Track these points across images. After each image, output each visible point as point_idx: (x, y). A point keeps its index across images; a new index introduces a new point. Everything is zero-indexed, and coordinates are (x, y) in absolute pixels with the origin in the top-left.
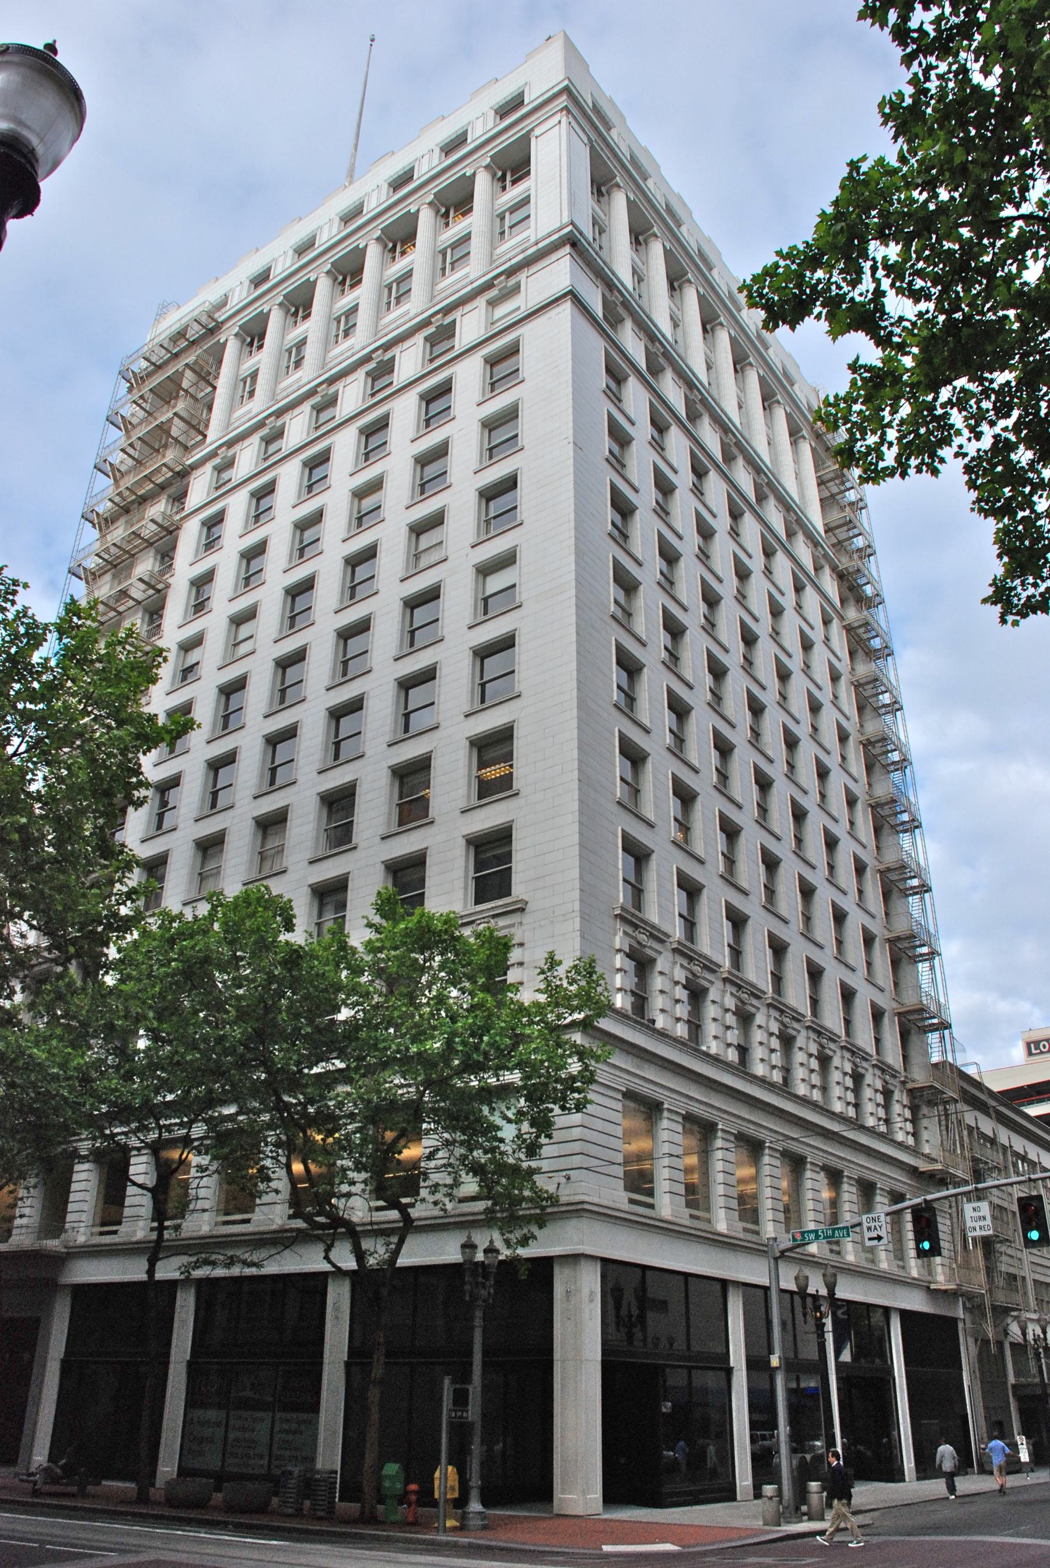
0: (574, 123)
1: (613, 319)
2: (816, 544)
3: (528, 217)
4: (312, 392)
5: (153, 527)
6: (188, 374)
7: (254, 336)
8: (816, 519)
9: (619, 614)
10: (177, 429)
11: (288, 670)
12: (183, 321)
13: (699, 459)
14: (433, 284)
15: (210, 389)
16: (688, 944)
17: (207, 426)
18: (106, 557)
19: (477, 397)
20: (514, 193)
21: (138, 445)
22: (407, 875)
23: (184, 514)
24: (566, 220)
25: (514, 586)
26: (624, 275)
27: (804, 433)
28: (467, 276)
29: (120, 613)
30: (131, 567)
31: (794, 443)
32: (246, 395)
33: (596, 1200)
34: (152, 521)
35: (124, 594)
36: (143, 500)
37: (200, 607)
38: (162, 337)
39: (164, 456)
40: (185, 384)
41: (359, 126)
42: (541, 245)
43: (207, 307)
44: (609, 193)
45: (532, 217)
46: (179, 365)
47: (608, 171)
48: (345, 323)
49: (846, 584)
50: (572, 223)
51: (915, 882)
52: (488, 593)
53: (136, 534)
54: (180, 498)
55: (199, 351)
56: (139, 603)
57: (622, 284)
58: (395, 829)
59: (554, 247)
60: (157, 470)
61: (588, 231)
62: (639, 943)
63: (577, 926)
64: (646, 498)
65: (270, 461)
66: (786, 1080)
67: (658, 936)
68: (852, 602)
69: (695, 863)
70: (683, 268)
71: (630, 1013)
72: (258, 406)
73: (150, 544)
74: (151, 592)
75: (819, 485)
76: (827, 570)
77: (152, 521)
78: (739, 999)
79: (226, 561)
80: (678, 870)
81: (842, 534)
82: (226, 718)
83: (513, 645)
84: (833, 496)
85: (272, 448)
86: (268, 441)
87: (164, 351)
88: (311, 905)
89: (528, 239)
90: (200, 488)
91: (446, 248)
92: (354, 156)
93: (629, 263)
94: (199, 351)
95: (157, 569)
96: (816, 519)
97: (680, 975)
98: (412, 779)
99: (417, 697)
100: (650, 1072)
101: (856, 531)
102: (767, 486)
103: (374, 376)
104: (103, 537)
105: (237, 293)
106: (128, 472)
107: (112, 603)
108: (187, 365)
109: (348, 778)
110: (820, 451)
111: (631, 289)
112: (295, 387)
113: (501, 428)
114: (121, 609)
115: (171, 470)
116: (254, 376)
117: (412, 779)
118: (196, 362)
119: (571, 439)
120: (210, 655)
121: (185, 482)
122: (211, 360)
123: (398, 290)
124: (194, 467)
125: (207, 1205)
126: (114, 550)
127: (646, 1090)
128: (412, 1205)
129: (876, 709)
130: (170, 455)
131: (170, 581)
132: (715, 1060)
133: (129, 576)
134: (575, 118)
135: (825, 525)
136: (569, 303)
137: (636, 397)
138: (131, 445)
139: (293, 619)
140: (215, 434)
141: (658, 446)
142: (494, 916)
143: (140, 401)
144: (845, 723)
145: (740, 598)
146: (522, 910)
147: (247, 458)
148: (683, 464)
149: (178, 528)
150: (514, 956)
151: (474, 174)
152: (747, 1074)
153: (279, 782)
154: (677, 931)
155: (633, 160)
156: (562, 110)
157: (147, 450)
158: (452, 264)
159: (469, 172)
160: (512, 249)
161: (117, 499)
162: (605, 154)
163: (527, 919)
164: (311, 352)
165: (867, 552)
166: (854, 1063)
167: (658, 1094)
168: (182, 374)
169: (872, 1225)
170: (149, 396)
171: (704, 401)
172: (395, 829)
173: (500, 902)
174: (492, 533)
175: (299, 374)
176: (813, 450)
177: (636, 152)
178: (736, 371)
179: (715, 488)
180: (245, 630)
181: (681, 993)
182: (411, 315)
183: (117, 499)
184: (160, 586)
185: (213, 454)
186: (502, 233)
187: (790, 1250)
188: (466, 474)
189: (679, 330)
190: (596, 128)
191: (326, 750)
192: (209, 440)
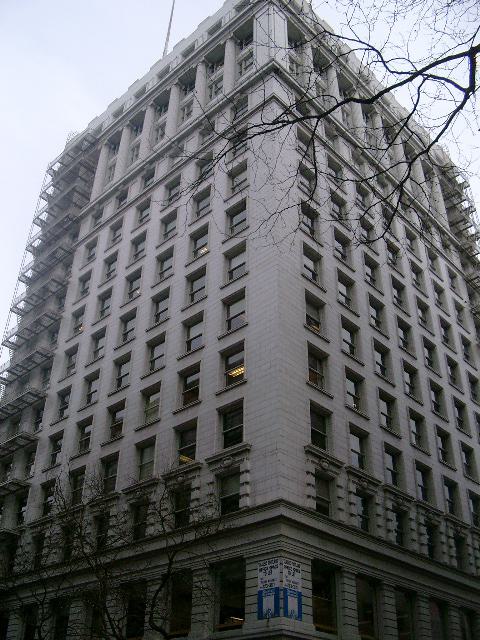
7: (114, 145)
20: (245, 51)
21: (56, 209)
33: (291, 629)
40: (80, 173)
54: (75, 236)
59: (266, 73)
66: (432, 548)
69: (362, 420)
74: (60, 287)
76: (452, 247)
88: (77, 434)
90: (85, 230)
97: (390, 505)
100: (408, 576)
101: (469, 224)
124: (82, 217)
125: (16, 634)
126: (41, 266)
149: (75, 251)
152: (331, 521)
163: (251, 455)
166: (456, 530)
167: (413, 587)
185: (92, 208)
186: (241, 72)
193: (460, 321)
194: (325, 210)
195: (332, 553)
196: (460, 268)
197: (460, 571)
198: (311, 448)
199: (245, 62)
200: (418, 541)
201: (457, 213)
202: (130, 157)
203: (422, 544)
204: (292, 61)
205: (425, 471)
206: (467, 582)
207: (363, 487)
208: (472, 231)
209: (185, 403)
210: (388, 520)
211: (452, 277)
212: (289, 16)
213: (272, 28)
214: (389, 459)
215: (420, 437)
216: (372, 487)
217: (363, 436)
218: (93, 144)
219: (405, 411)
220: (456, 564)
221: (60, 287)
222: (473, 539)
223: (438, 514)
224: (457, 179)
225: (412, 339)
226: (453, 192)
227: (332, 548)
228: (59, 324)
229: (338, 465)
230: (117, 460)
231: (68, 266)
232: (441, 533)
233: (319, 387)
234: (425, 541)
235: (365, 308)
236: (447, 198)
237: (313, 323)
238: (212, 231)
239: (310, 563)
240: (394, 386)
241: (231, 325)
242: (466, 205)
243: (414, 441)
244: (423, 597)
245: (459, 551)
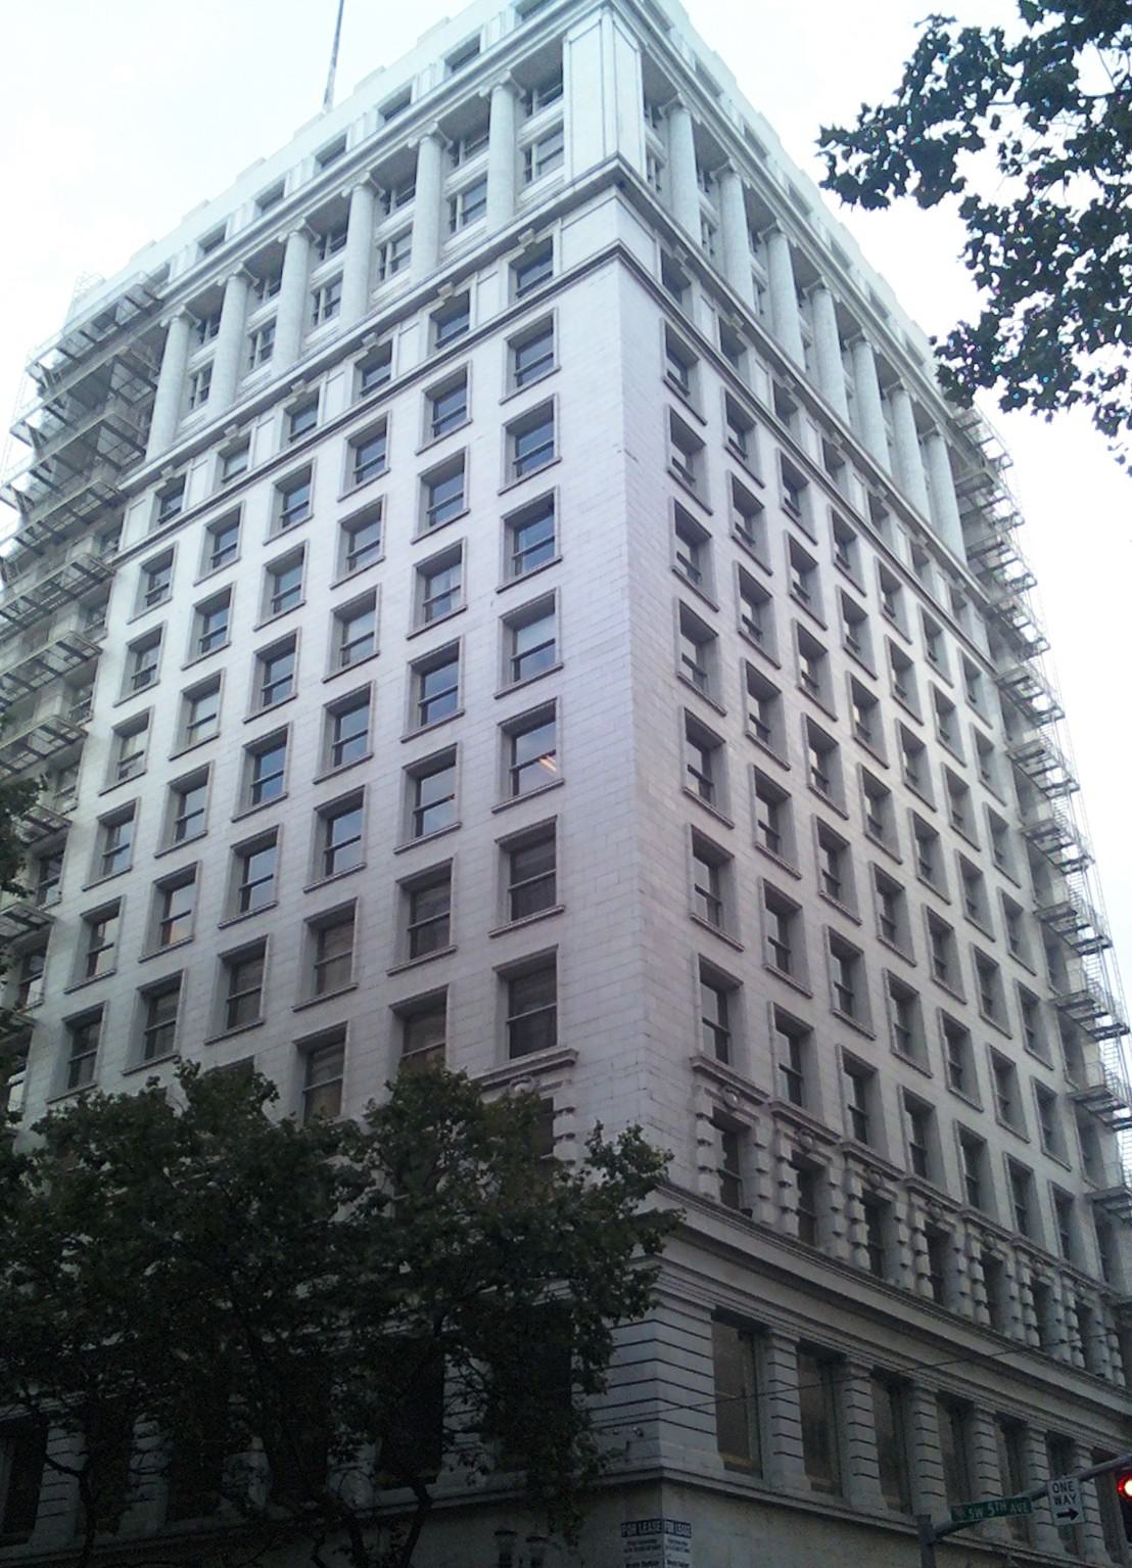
1: (675, 281)
2: (955, 574)
3: (561, 149)
4: (285, 391)
5: (77, 574)
6: (119, 369)
7: (205, 318)
8: (954, 541)
9: (688, 673)
10: (106, 442)
11: (264, 760)
12: (111, 299)
14: (442, 242)
15: (148, 389)
17: (146, 439)
18: (13, 614)
19: (500, 395)
20: (543, 119)
21: (54, 465)
22: (421, 1017)
23: (117, 556)
24: (611, 152)
25: (552, 642)
26: (691, 228)
28: (482, 231)
29: (34, 690)
30: (47, 628)
31: (924, 442)
32: (198, 396)
33: (680, 1466)
34: (75, 565)
35: (39, 662)
36: (62, 539)
37: (142, 679)
38: (84, 319)
39: (88, 479)
40: (115, 383)
41: (338, 34)
42: (579, 186)
43: (141, 279)
44: (668, 115)
45: (567, 150)
46: (106, 358)
47: (664, 92)
48: (324, 300)
49: (997, 626)
50: (618, 156)
51: (1107, 1021)
52: (520, 652)
53: (53, 584)
55: (132, 339)
56: (59, 675)
58: (405, 962)
60: (81, 498)
61: (639, 164)
64: (720, 522)
65: (233, 485)
68: (1007, 650)
70: (771, 213)
71: (718, 1201)
72: (213, 412)
73: (72, 596)
74: (76, 660)
75: (958, 496)
76: (971, 608)
77: (75, 565)
79: (177, 617)
83: (553, 719)
85: (234, 467)
86: (227, 457)
87: (85, 340)
89: (561, 179)
90: (138, 524)
91: (455, 195)
92: (331, 74)
93: (697, 207)
94: (132, 339)
95: (82, 630)
96: (954, 541)
97: (786, 1150)
98: (426, 893)
99: (432, 787)
100: (901, 1345)
102: (885, 503)
103: (366, 369)
104: (9, 587)
105: (181, 261)
106: (42, 502)
107: (22, 676)
108: (117, 357)
109: (344, 898)
111: (699, 243)
112: (261, 386)
113: (531, 438)
114: (34, 684)
115: (99, 497)
116: (207, 372)
117: (426, 893)
118: (129, 353)
119: (622, 447)
120: (161, 738)
121: (118, 513)
122: (149, 352)
123: (389, 255)
126: (22, 605)
127: (746, 1308)
128: (432, 1480)
129: (1044, 790)
130: (97, 479)
131: (102, 645)
133: (46, 640)
135: (968, 549)
137: (710, 387)
138: (44, 465)
139: (268, 692)
140: (157, 450)
142: (535, 1073)
143: (55, 407)
144: (999, 810)
146: (571, 1063)
147: (201, 481)
148: (770, 472)
149: (112, 574)
150: (561, 1125)
151: (490, 95)
153: (253, 906)
155: (701, 71)
157: (67, 473)
158: (465, 215)
159: (483, 92)
160: (544, 190)
161: (26, 538)
162: (663, 64)
163: (578, 1075)
164: (282, 338)
165: (1022, 584)
167: (761, 1314)
168: (111, 370)
169: (1062, 1494)
170: (66, 400)
172: (405, 962)
173: (543, 1054)
174: (524, 574)
175: (267, 367)
176: (951, 450)
178: (843, 348)
180: (205, 709)
181: (790, 1175)
182: (412, 285)
183: (26, 538)
184: (88, 653)
185: (155, 476)
187: (949, 1531)
188: (488, 498)
189: (766, 296)
190: (649, 28)
191: (315, 861)
192: (149, 456)
193: (986, 777)
194: (720, 522)
196: (987, 655)
197: (992, 1333)
198: (853, 1145)
199: (532, 159)
201: (985, 531)
202: (247, 354)
203: (785, 1210)
206: (1012, 1360)
207: (806, 1150)
209: (413, 955)
210: (783, 1184)
211: (971, 676)
214: (783, 1042)
215: (960, 1071)
216: (748, 1107)
219: (753, 889)
220: (1123, 1383)
222: (911, 1205)
223: (826, 1138)
224: (985, 447)
225: (716, 667)
228: (80, 750)
230: (99, 1020)
232: (957, 1250)
234: (794, 1204)
235: (800, 751)
236: (962, 493)
239: (792, 1349)
240: (858, 924)
243: (837, 1005)
244: (925, 1391)
245: (876, 1234)
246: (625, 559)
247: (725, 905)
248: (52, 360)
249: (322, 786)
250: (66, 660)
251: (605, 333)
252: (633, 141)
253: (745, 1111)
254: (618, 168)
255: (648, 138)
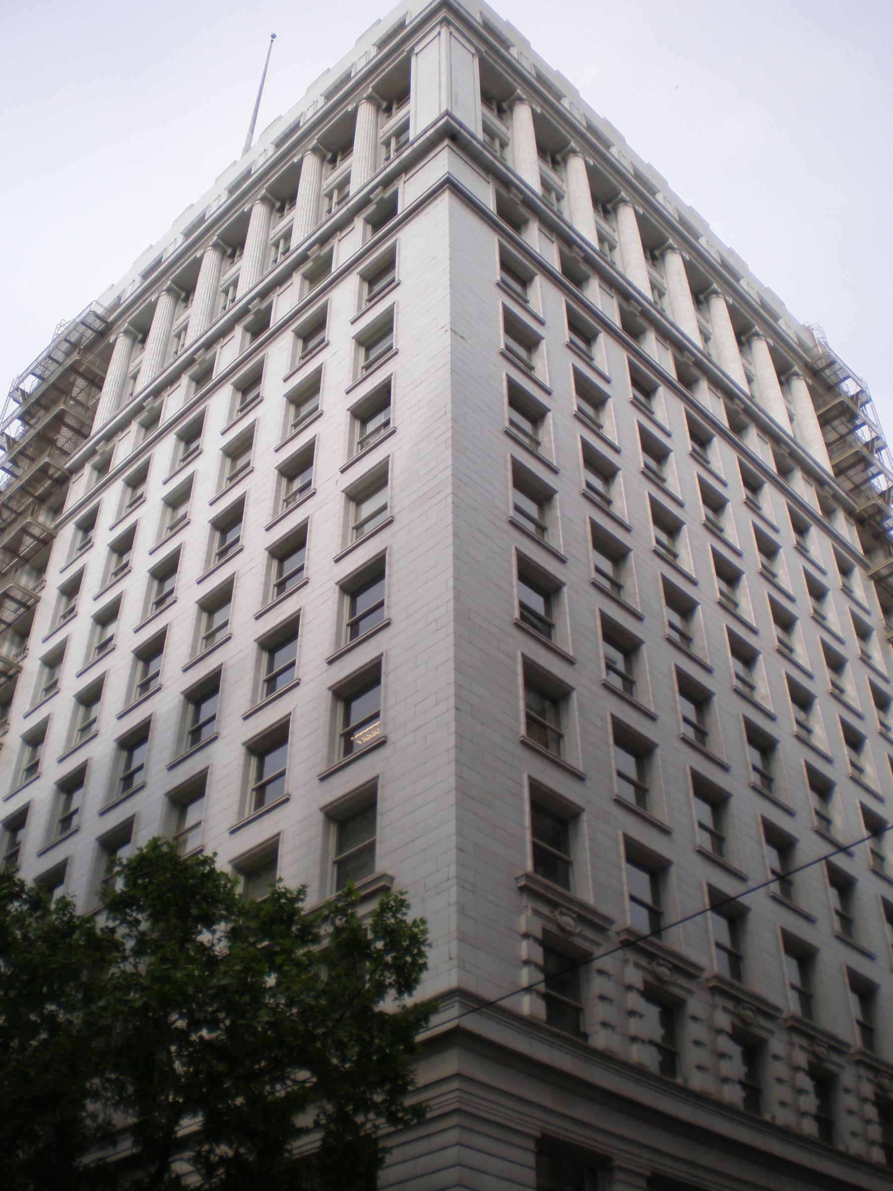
0: (455, 33)
13: (701, 427)
16: (806, 1020)
24: (443, 110)
27: (796, 368)
40: (75, 391)
56: (9, 625)
57: (582, 239)
62: (560, 927)
63: (453, 897)
67: (767, 1011)
71: (742, 1108)
74: (22, 610)
78: (814, 1054)
80: (530, 778)
81: (856, 475)
82: (260, 790)
84: (842, 437)
90: (77, 492)
96: (815, 446)
101: (873, 470)
109: (199, 768)
110: (819, 389)
113: (376, 339)
119: (448, 327)
120: (304, 756)
132: (785, 1134)
134: (457, 29)
136: (447, 193)
141: (753, 506)
145: (865, 658)
154: (791, 1005)
156: (440, 22)
171: (747, 411)
176: (811, 389)
177: (763, 296)
179: (772, 502)
181: (804, 1081)
189: (754, 384)
195: (587, 1126)
200: (788, 1099)
204: (487, 129)
205: (802, 954)
207: (659, 979)
208: (881, 484)
212: (483, 49)
213: (443, 81)
217: (654, 868)
218: (102, 334)
221: (22, 610)
226: (840, 412)
227: (584, 1112)
229: (596, 922)
231: (40, 570)
233: (552, 752)
237: (537, 625)
238: (314, 540)
239: (531, 1145)
241: (347, 746)
242: (865, 434)
246: (449, 416)
247: (566, 738)
248: (30, 384)
249: (190, 671)
250: (15, 612)
251: (438, 251)
252: (472, 116)
253: (678, 986)
254: (447, 122)
255: (483, 114)
